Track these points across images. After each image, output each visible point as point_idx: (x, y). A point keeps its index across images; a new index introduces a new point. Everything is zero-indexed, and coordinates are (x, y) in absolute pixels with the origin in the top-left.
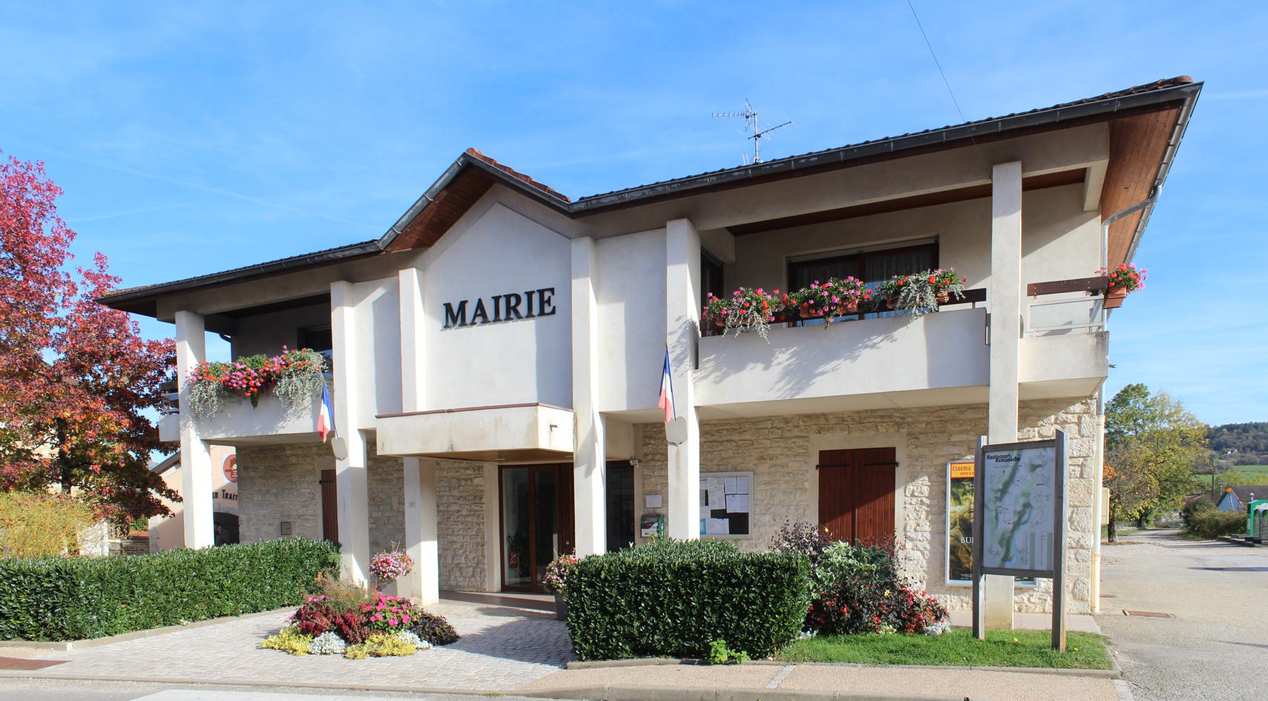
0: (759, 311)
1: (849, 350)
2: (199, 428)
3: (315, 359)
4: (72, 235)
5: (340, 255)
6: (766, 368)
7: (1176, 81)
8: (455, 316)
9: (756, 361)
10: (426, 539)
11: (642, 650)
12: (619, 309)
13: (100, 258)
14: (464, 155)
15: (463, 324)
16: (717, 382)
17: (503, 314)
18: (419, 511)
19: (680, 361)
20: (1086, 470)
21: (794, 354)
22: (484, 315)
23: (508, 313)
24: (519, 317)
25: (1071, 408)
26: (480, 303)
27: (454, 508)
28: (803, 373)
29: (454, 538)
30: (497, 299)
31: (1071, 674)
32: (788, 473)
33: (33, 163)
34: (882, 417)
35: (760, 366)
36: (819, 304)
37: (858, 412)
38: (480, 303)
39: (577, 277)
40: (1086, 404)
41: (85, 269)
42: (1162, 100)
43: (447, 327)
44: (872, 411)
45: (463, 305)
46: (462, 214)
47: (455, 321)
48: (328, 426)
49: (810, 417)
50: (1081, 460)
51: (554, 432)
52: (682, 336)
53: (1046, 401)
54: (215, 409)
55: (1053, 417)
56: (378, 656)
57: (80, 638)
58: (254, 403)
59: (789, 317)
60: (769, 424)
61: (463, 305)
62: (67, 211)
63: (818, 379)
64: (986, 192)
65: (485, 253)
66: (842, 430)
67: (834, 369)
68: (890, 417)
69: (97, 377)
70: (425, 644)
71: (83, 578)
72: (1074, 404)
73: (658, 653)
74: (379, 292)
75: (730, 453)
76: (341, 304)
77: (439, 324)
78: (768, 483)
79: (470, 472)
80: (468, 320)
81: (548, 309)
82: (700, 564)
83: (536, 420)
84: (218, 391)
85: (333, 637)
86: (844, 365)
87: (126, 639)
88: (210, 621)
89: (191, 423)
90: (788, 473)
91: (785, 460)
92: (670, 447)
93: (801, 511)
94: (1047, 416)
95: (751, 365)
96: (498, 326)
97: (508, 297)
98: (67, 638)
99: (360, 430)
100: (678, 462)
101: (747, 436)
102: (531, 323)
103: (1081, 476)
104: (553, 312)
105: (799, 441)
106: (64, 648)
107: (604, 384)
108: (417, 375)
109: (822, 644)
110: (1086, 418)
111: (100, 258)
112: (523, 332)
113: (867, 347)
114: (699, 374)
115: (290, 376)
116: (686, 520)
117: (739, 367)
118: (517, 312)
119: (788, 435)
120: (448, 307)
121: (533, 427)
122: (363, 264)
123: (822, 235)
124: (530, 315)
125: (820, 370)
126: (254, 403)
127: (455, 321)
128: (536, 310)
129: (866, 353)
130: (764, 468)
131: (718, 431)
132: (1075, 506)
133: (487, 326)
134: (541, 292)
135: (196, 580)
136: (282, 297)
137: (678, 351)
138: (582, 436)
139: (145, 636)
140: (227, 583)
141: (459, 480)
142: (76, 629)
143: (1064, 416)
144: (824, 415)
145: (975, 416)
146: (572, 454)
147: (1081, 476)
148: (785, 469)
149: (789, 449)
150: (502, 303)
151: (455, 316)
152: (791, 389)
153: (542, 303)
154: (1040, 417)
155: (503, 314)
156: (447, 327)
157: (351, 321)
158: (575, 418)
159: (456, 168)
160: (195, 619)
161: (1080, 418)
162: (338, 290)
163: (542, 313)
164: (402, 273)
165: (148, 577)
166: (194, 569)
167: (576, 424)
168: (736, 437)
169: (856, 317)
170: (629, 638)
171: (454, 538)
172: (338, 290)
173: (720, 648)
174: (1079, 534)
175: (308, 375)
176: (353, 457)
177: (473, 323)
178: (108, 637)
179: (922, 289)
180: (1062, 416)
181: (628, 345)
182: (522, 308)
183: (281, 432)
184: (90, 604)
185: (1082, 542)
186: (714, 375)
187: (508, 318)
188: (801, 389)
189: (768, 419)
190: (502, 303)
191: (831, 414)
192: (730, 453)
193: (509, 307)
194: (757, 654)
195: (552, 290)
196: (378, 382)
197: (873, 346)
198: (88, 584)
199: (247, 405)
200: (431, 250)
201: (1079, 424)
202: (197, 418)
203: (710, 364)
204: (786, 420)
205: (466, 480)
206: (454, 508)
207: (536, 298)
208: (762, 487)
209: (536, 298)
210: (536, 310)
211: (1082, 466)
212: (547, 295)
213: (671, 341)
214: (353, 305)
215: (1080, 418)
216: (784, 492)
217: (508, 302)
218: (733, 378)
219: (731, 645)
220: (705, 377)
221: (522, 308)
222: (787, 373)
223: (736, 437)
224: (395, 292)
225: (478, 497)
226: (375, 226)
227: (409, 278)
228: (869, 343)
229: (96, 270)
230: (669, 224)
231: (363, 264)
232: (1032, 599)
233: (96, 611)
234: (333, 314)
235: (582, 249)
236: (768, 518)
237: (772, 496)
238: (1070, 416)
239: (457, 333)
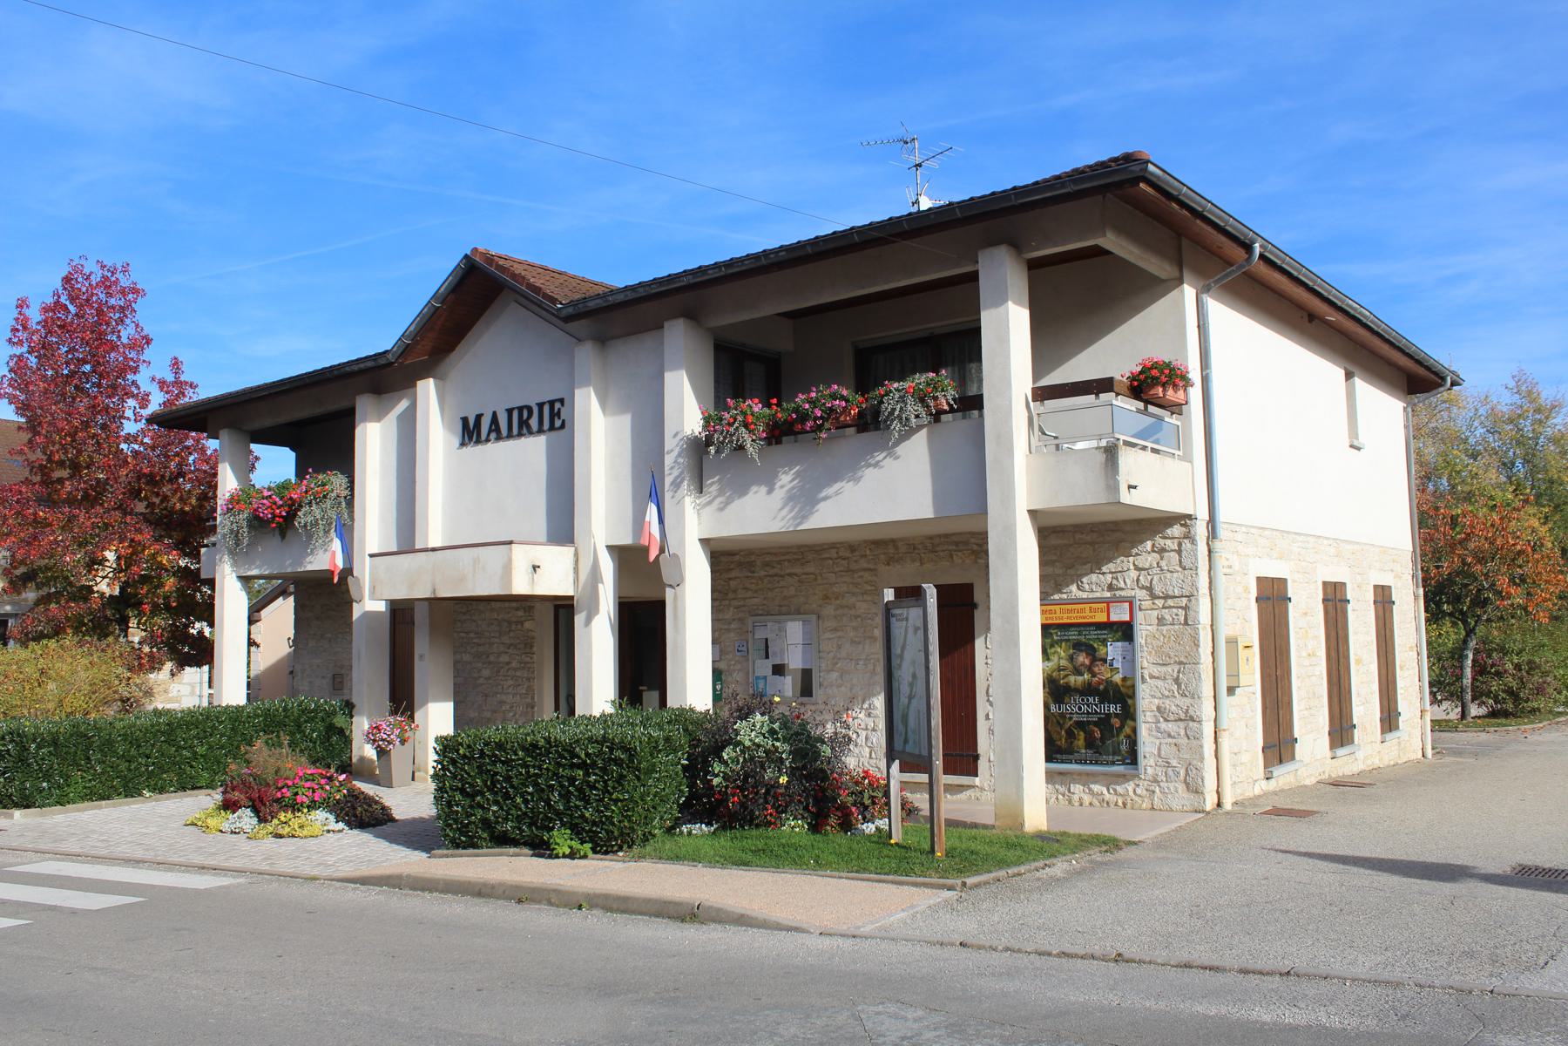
0: (746, 426)
1: (849, 470)
2: (235, 564)
3: (337, 481)
4: (148, 342)
5: (355, 368)
6: (770, 492)
7: (1128, 158)
8: (471, 432)
9: (759, 484)
10: (436, 700)
11: (502, 840)
12: (626, 421)
13: (176, 365)
14: (466, 256)
15: (478, 441)
16: (721, 509)
17: (515, 430)
18: (430, 667)
19: (677, 485)
20: (1191, 613)
21: (797, 475)
22: (498, 430)
23: (520, 428)
24: (531, 433)
25: (1169, 531)
26: (495, 414)
27: (504, 658)
28: (806, 498)
29: (504, 698)
30: (510, 411)
31: (907, 884)
32: (857, 617)
33: (119, 267)
34: (957, 544)
35: (763, 489)
36: (804, 417)
37: (931, 538)
38: (495, 414)
39: (580, 387)
40: (1185, 525)
41: (158, 376)
42: (1116, 178)
43: (463, 444)
44: (947, 536)
45: (479, 417)
46: (481, 315)
47: (470, 439)
48: (340, 563)
49: (877, 543)
50: (1185, 600)
51: (544, 571)
52: (679, 455)
53: (1139, 522)
54: (246, 542)
55: (1149, 544)
56: (281, 836)
57: (27, 807)
58: (283, 536)
59: (778, 433)
60: (833, 553)
61: (479, 417)
62: (147, 316)
63: (822, 506)
64: (973, 277)
65: (498, 362)
66: (913, 561)
67: (837, 493)
68: (966, 543)
69: (165, 498)
70: (341, 825)
71: (34, 741)
72: (1171, 526)
73: (514, 843)
74: (403, 405)
75: (792, 591)
76: (364, 420)
77: (456, 441)
78: (836, 630)
79: (520, 613)
80: (483, 437)
81: (558, 423)
82: (548, 740)
83: (510, 560)
84: (249, 521)
85: (248, 811)
86: (845, 487)
87: (78, 810)
88: (180, 793)
89: (226, 558)
90: (857, 617)
91: (853, 599)
92: (668, 590)
93: (870, 667)
94: (1142, 542)
95: (754, 488)
96: (511, 443)
97: (521, 409)
98: (17, 806)
99: (240, 578)
100: (675, 608)
101: (810, 568)
102: (542, 439)
103: (1186, 623)
104: (563, 426)
105: (866, 575)
106: (12, 816)
107: (605, 514)
108: (436, 505)
109: (724, 840)
110: (1187, 544)
111: (176, 365)
112: (533, 450)
113: (869, 466)
114: (704, 499)
115: (310, 504)
116: (693, 682)
117: (742, 491)
118: (529, 427)
119: (854, 566)
120: (465, 420)
121: (507, 568)
122: (383, 377)
123: (832, 334)
124: (540, 431)
125: (823, 494)
126: (283, 536)
127: (470, 439)
128: (546, 425)
129: (869, 473)
130: (829, 610)
131: (779, 562)
132: (1181, 663)
133: (501, 444)
134: (552, 403)
135: (165, 746)
136: (318, 411)
137: (676, 472)
138: (583, 577)
139: (100, 808)
140: (200, 750)
141: (510, 623)
142: (24, 797)
143: (1162, 542)
144: (893, 541)
145: (1060, 542)
146: (572, 598)
147: (1186, 623)
148: (853, 612)
149: (856, 585)
150: (515, 414)
151: (471, 432)
152: (794, 518)
153: (550, 418)
154: (1134, 544)
155: (515, 430)
156: (463, 444)
157: (374, 440)
158: (576, 554)
159: (460, 272)
160: (162, 790)
161: (1180, 545)
162: (363, 404)
163: (552, 428)
164: (420, 383)
165: (110, 743)
166: (163, 733)
167: (577, 562)
168: (798, 570)
169: (852, 430)
170: (485, 822)
171: (504, 698)
172: (363, 404)
173: (562, 839)
174: (1188, 701)
175: (329, 503)
176: (370, 604)
177: (488, 440)
178: (59, 807)
179: (902, 399)
180: (1160, 541)
181: (634, 465)
182: (534, 422)
183: (310, 568)
184: (40, 769)
185: (1191, 712)
186: (716, 504)
187: (520, 435)
188: (805, 518)
189: (833, 546)
190: (515, 414)
191: (901, 540)
192: (792, 591)
193: (520, 422)
194: (603, 847)
195: (562, 401)
196: (399, 511)
197: (876, 465)
198: (39, 747)
199: (276, 540)
200: (453, 356)
201: (1179, 552)
202: (232, 553)
203: (715, 487)
204: (852, 548)
205: (517, 623)
206: (504, 658)
207: (546, 409)
208: (828, 635)
209: (546, 409)
210: (546, 425)
211: (1186, 608)
212: (557, 405)
213: (669, 460)
214: (379, 420)
215: (1180, 545)
216: (853, 642)
217: (520, 415)
218: (738, 504)
219: (576, 831)
220: (710, 503)
221: (534, 422)
222: (790, 498)
223: (798, 570)
224: (413, 407)
225: (528, 645)
226: (381, 335)
227: (427, 389)
228: (872, 461)
229: (170, 378)
230: (666, 324)
231: (383, 377)
232: (1139, 791)
233: (47, 776)
234: (358, 431)
235: (586, 354)
236: (835, 675)
237: (839, 647)
238: (1168, 542)
239: (473, 451)
